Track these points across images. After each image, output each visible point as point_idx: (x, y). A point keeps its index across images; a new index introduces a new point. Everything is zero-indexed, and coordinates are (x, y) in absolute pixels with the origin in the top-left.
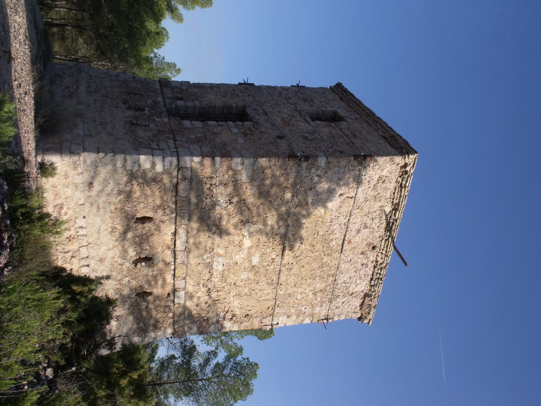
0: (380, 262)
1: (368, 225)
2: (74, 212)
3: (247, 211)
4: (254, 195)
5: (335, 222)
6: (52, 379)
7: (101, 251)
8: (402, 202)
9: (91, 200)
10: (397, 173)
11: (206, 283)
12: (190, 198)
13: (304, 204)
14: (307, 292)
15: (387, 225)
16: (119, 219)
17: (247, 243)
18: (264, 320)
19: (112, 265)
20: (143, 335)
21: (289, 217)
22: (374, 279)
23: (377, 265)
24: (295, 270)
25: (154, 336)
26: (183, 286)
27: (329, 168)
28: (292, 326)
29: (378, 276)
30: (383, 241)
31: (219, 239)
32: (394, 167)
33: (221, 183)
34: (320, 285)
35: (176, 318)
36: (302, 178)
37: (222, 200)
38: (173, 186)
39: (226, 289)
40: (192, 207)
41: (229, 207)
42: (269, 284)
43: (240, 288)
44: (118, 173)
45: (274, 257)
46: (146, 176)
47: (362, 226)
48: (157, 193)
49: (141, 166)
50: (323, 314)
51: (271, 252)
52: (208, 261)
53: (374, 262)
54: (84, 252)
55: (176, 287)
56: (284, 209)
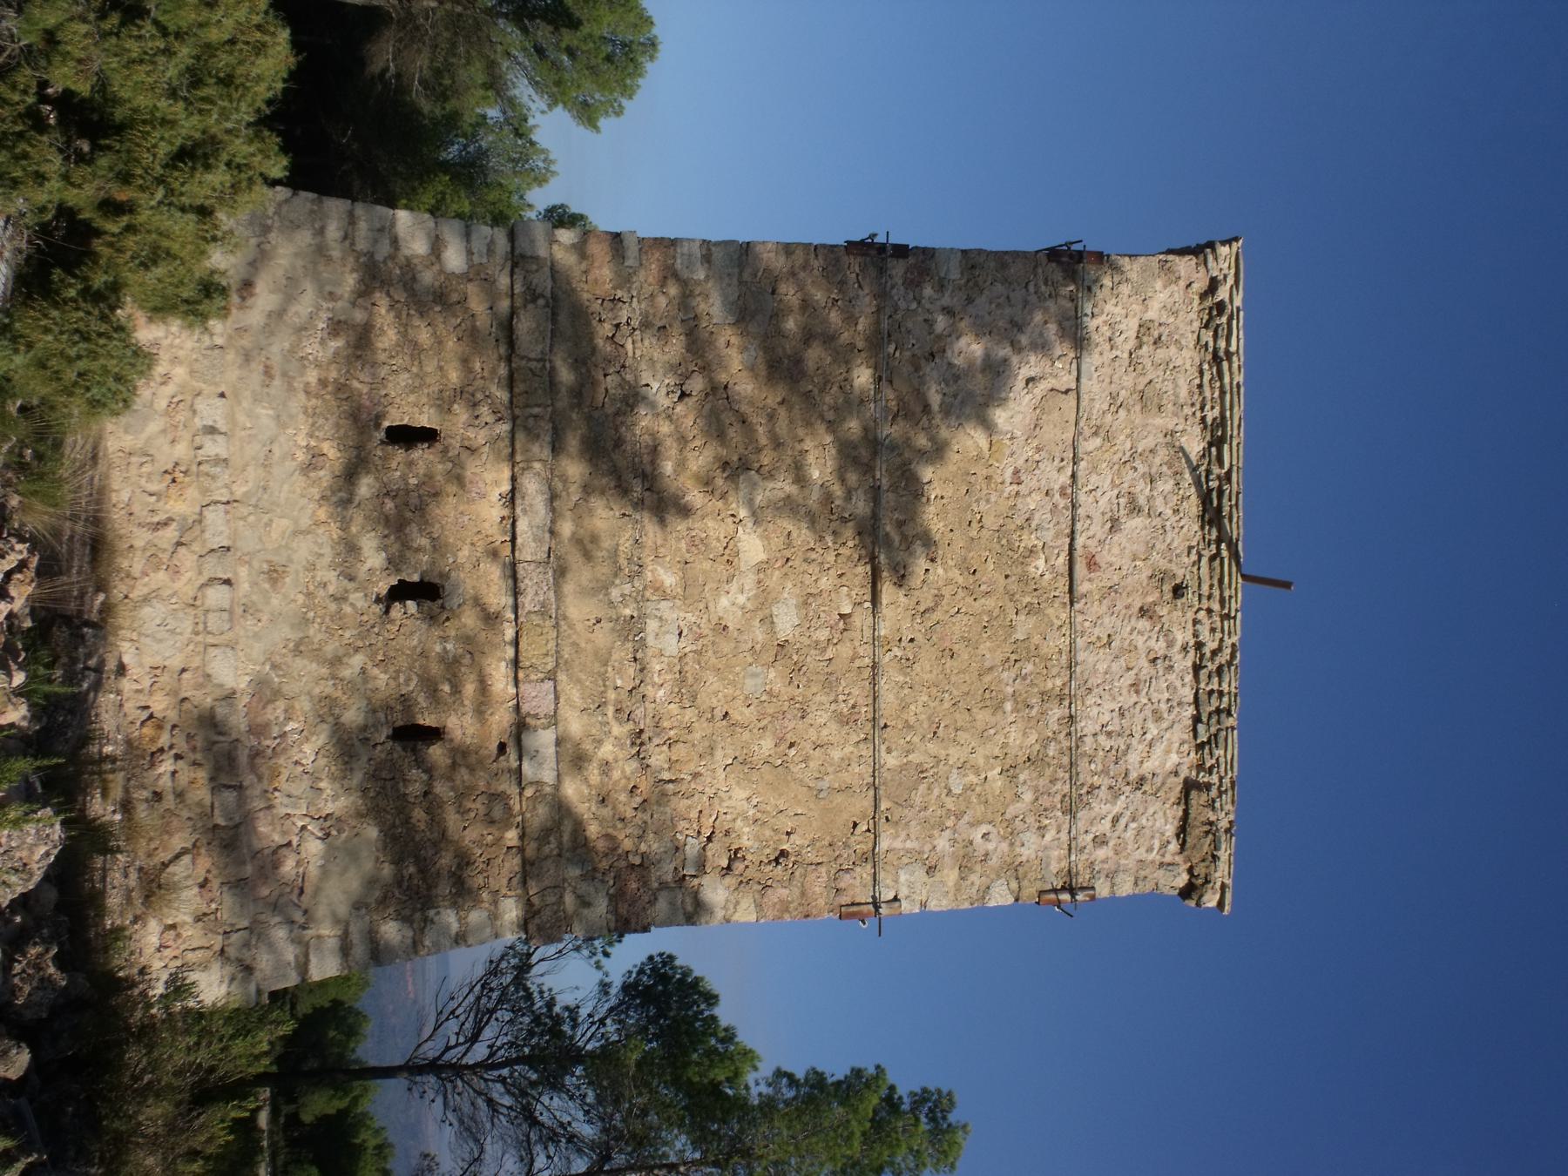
0: (1211, 645)
1: (1142, 501)
2: (192, 372)
3: (737, 426)
4: (752, 369)
5: (1029, 482)
6: (66, 987)
7: (274, 535)
8: (1231, 409)
9: (246, 342)
10: (1193, 315)
11: (627, 704)
12: (553, 369)
13: (914, 410)
14: (981, 762)
15: (1204, 503)
16: (333, 420)
17: (752, 547)
18: (845, 881)
19: (309, 595)
20: (418, 915)
21: (875, 454)
22: (1205, 719)
23: (1202, 656)
24: (925, 668)
25: (455, 927)
26: (546, 706)
27: (976, 284)
28: (951, 913)
29: (1215, 702)
30: (1204, 561)
31: (657, 528)
32: (1178, 290)
33: (646, 325)
34: (1019, 739)
35: (530, 851)
36: (898, 317)
37: (658, 387)
38: (500, 324)
39: (697, 735)
40: (563, 402)
41: (679, 408)
42: (845, 721)
43: (746, 736)
44: (329, 259)
45: (846, 610)
46: (414, 279)
47: (1122, 501)
48: (451, 343)
49: (401, 243)
50: (1054, 867)
51: (837, 588)
52: (628, 612)
53: (1192, 652)
54: (217, 527)
55: (525, 708)
56: (853, 426)
